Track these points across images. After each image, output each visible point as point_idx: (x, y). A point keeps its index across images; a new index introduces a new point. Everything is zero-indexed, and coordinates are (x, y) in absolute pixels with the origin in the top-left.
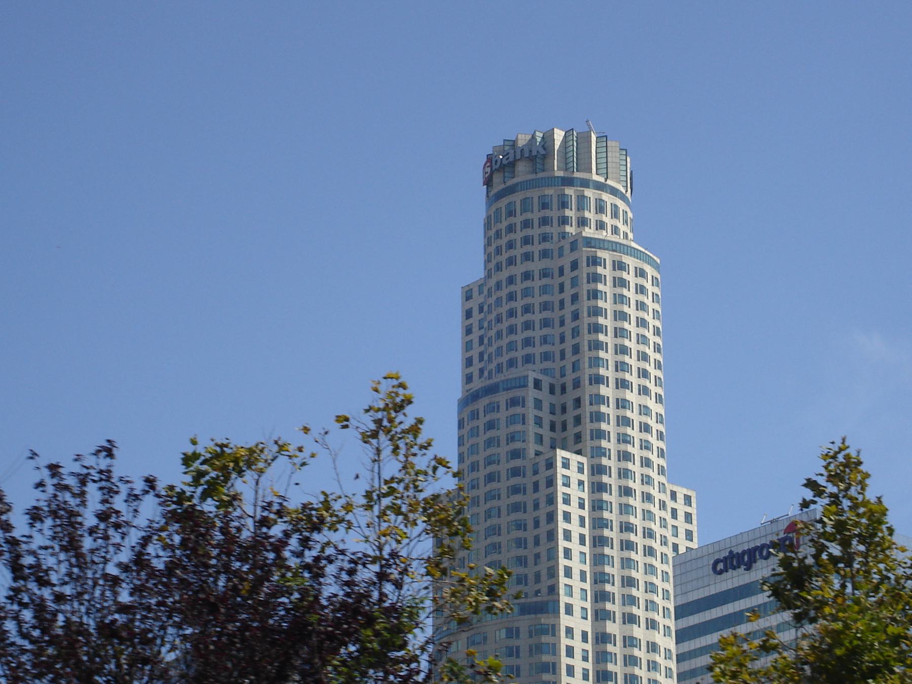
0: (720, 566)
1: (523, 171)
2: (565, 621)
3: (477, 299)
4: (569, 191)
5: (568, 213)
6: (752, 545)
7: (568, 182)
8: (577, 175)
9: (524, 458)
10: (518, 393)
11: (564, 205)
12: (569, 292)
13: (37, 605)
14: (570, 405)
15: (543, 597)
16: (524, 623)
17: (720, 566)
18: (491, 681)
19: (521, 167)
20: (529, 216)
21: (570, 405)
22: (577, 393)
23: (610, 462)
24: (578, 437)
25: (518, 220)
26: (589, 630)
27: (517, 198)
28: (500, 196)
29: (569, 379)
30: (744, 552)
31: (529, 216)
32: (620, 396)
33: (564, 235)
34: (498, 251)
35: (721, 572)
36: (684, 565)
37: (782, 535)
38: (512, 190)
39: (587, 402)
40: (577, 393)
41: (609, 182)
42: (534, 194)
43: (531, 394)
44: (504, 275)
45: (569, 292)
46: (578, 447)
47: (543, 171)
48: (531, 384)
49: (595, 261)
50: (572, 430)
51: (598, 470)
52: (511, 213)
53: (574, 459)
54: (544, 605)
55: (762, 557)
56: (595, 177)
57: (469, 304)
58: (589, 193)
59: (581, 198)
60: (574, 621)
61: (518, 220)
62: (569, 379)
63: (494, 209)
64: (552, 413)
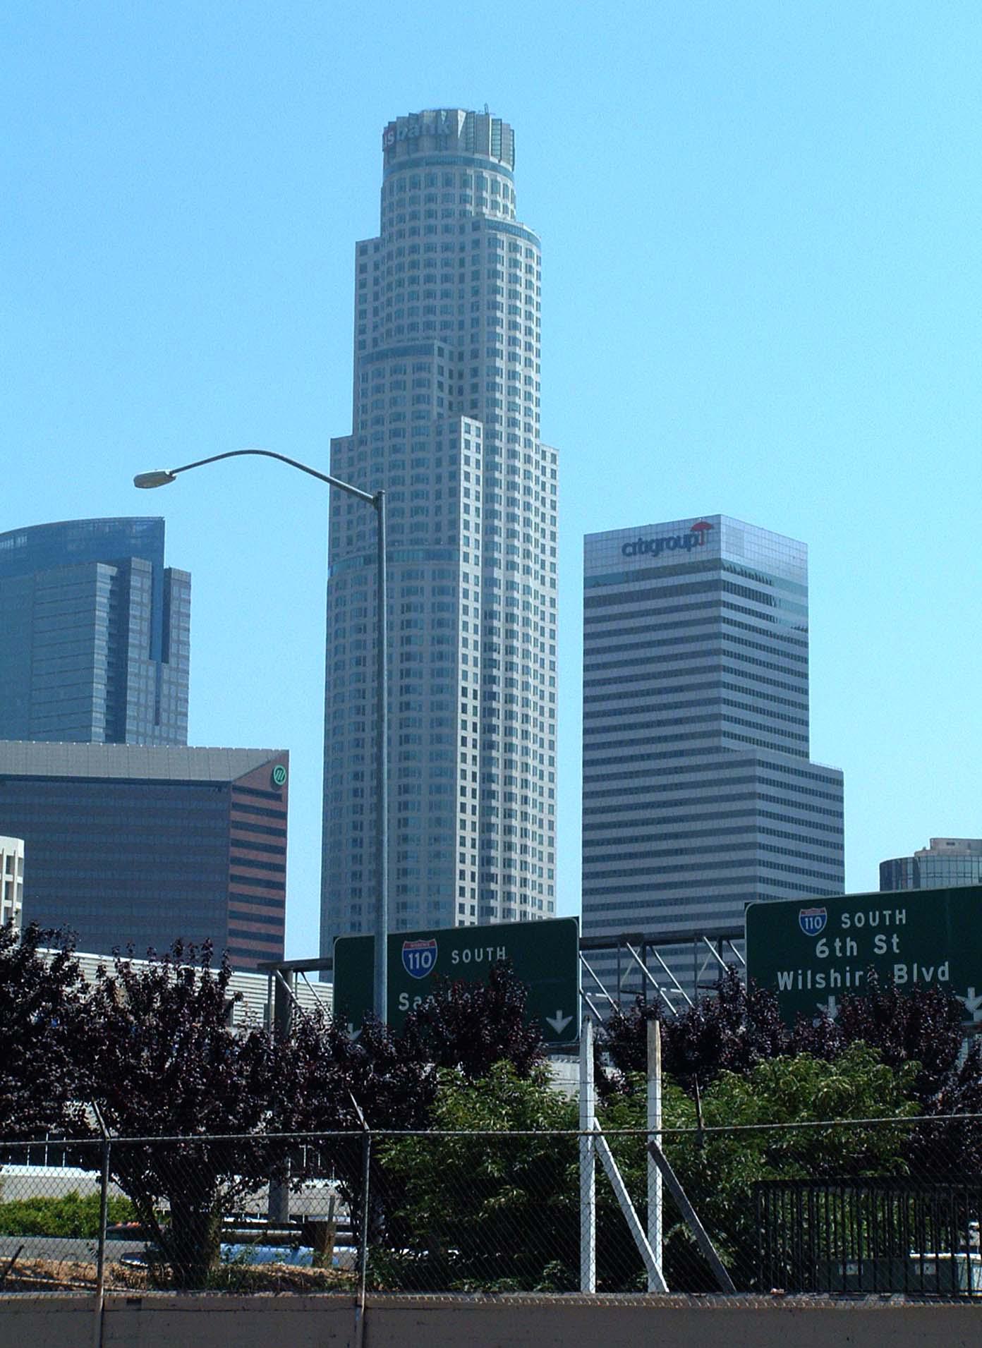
0: (630, 550)
1: (427, 149)
2: (464, 567)
3: (372, 256)
4: (470, 172)
5: (468, 192)
6: (660, 537)
7: (469, 162)
8: (477, 156)
9: (429, 419)
10: (424, 359)
11: (465, 184)
12: (469, 269)
13: (711, 1033)
14: (467, 372)
15: (443, 546)
16: (429, 567)
17: (630, 550)
18: (973, 1056)
19: (426, 143)
20: (433, 190)
21: (467, 372)
22: (475, 363)
23: (501, 428)
24: (474, 405)
25: (422, 193)
26: (480, 574)
27: (421, 172)
28: (402, 166)
29: (467, 348)
30: (653, 541)
31: (433, 190)
32: (511, 368)
33: (464, 214)
34: (401, 219)
35: (629, 555)
36: (593, 543)
37: (688, 532)
38: (416, 163)
39: (485, 373)
40: (475, 363)
41: (502, 163)
42: (438, 171)
43: (437, 360)
44: (407, 243)
45: (469, 269)
46: (475, 412)
47: (447, 149)
48: (436, 352)
49: (494, 243)
50: (468, 396)
51: (491, 435)
52: (415, 185)
53: (475, 424)
54: (447, 552)
55: (669, 548)
56: (492, 159)
57: (364, 259)
58: (486, 174)
59: (480, 178)
60: (470, 568)
61: (422, 193)
62: (467, 348)
63: (395, 177)
64: (451, 377)
